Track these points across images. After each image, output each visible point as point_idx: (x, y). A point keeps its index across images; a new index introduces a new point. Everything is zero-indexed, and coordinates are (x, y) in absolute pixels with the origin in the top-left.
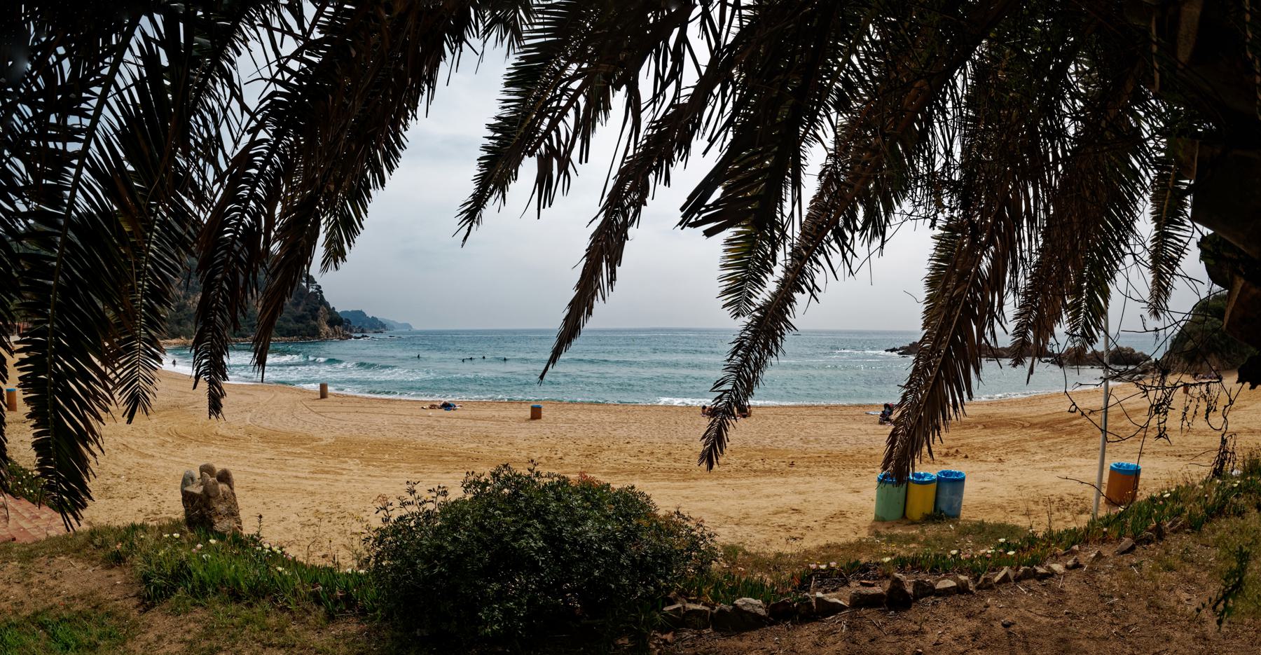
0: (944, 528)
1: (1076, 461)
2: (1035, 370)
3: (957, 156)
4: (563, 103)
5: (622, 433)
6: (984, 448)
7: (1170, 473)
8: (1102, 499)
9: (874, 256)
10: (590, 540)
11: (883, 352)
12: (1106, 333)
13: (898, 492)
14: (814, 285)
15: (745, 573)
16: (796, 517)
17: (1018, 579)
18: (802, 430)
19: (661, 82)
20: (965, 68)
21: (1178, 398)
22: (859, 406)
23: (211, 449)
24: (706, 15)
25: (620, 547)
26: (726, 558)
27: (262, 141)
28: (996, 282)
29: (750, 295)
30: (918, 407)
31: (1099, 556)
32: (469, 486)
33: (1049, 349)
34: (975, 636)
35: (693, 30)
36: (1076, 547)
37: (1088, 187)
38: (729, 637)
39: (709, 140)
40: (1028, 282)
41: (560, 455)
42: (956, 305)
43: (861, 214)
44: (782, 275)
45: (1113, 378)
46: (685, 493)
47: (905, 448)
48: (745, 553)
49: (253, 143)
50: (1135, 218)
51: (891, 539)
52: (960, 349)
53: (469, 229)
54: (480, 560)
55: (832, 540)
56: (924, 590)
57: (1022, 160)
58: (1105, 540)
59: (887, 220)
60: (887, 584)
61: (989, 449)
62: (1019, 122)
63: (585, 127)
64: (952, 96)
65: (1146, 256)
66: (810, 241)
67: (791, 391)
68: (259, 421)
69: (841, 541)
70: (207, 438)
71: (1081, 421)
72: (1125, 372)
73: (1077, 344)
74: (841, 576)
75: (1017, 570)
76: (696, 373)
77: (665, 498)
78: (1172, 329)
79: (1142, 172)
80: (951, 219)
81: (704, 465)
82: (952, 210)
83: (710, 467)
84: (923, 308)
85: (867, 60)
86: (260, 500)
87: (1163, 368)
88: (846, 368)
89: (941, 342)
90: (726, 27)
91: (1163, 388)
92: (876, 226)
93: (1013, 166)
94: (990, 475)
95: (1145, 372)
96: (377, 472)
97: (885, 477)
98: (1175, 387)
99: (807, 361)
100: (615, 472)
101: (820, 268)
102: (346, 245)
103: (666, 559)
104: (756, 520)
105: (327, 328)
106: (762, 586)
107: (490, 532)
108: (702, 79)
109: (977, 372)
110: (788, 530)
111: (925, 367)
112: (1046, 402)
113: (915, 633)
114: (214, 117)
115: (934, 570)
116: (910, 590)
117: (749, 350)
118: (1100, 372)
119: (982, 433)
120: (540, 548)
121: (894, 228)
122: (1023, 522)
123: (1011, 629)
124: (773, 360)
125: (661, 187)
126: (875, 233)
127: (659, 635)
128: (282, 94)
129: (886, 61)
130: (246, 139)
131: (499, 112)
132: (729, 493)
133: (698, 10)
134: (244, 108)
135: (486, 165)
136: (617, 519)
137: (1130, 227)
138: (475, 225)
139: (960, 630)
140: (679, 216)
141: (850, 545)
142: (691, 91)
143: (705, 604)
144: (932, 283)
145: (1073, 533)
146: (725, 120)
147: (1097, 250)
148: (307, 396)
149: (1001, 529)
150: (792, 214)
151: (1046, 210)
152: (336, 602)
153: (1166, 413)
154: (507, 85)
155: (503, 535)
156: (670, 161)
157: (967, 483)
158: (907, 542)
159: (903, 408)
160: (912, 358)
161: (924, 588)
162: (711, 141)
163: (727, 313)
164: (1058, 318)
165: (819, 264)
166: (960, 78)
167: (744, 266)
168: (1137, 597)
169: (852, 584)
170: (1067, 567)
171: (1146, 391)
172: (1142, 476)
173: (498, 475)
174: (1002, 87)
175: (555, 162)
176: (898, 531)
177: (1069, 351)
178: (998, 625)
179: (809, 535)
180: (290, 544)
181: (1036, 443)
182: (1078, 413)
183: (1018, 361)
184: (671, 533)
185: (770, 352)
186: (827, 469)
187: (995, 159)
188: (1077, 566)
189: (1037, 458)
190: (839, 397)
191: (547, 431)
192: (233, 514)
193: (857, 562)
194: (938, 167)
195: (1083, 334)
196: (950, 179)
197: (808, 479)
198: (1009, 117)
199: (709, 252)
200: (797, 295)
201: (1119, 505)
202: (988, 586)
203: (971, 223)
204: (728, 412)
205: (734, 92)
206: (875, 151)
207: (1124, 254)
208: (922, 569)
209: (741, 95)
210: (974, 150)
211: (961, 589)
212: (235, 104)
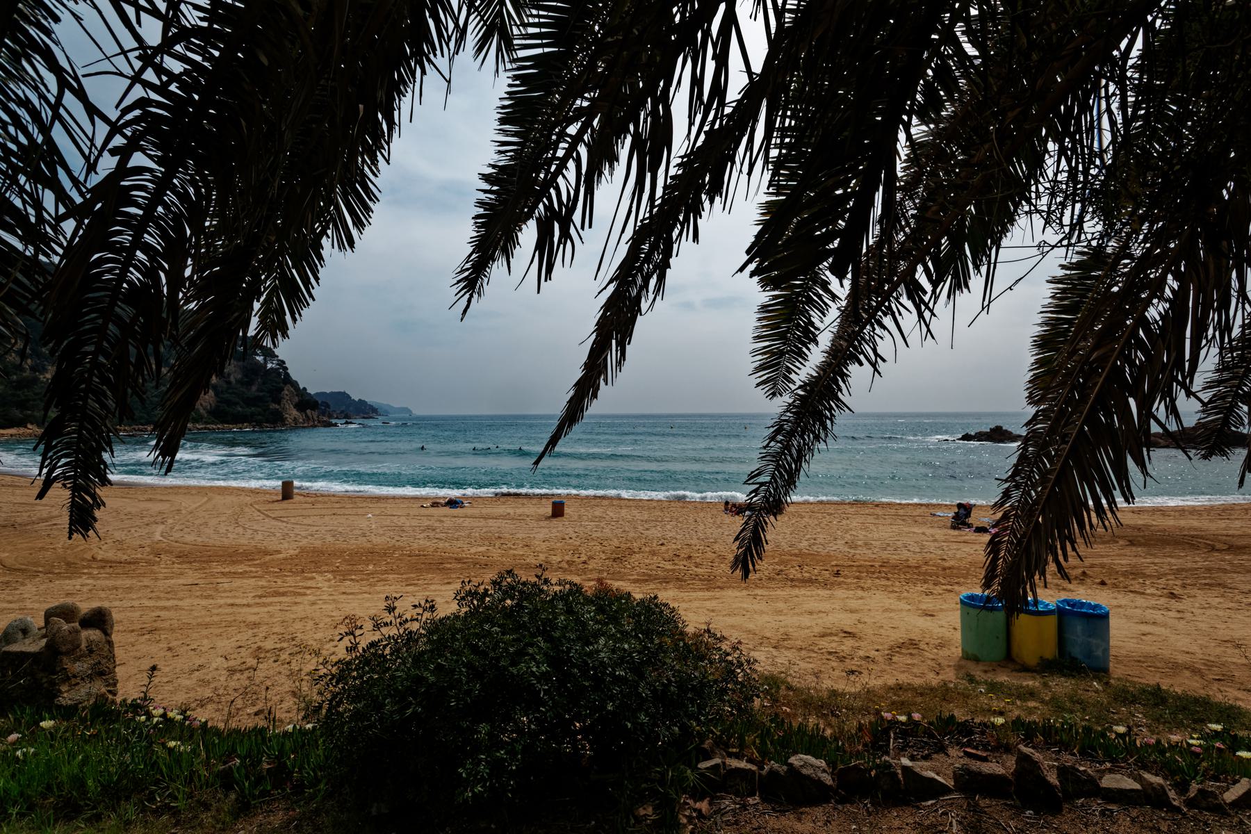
4: (560, 153)
5: (655, 533)
6: (1135, 573)
10: (602, 663)
16: (849, 643)
18: (847, 532)
23: (79, 581)
25: (638, 670)
27: (140, 170)
29: (789, 370)
32: (463, 598)
38: (783, 812)
41: (584, 558)
46: (708, 604)
48: (789, 688)
49: (122, 170)
53: (469, 301)
54: (468, 693)
55: (904, 678)
56: (1082, 787)
60: (1011, 762)
61: (1145, 576)
63: (590, 180)
68: (177, 535)
69: (917, 682)
70: (71, 568)
74: (932, 736)
77: (695, 611)
81: (738, 573)
86: (164, 645)
96: (356, 588)
100: (646, 579)
102: (288, 317)
104: (799, 643)
105: (295, 412)
107: (484, 654)
110: (842, 659)
111: (1038, 455)
114: (35, 115)
116: (1053, 778)
117: (791, 434)
119: (1127, 551)
120: (543, 674)
127: (690, 802)
128: (159, 105)
130: (108, 164)
131: (493, 158)
132: (762, 606)
134: (93, 111)
135: (483, 225)
136: (636, 637)
138: (475, 296)
141: (932, 689)
143: (750, 761)
144: (1043, 343)
148: (261, 498)
152: (260, 780)
154: (503, 121)
155: (498, 659)
157: (1114, 622)
163: (761, 393)
165: (884, 328)
167: (782, 336)
169: (954, 752)
173: (499, 584)
175: (556, 226)
180: (202, 704)
184: (702, 658)
185: (817, 438)
186: (884, 582)
191: (570, 530)
192: (101, 674)
197: (860, 593)
200: (853, 368)
208: (1066, 746)
211: (1152, 798)
212: (69, 99)
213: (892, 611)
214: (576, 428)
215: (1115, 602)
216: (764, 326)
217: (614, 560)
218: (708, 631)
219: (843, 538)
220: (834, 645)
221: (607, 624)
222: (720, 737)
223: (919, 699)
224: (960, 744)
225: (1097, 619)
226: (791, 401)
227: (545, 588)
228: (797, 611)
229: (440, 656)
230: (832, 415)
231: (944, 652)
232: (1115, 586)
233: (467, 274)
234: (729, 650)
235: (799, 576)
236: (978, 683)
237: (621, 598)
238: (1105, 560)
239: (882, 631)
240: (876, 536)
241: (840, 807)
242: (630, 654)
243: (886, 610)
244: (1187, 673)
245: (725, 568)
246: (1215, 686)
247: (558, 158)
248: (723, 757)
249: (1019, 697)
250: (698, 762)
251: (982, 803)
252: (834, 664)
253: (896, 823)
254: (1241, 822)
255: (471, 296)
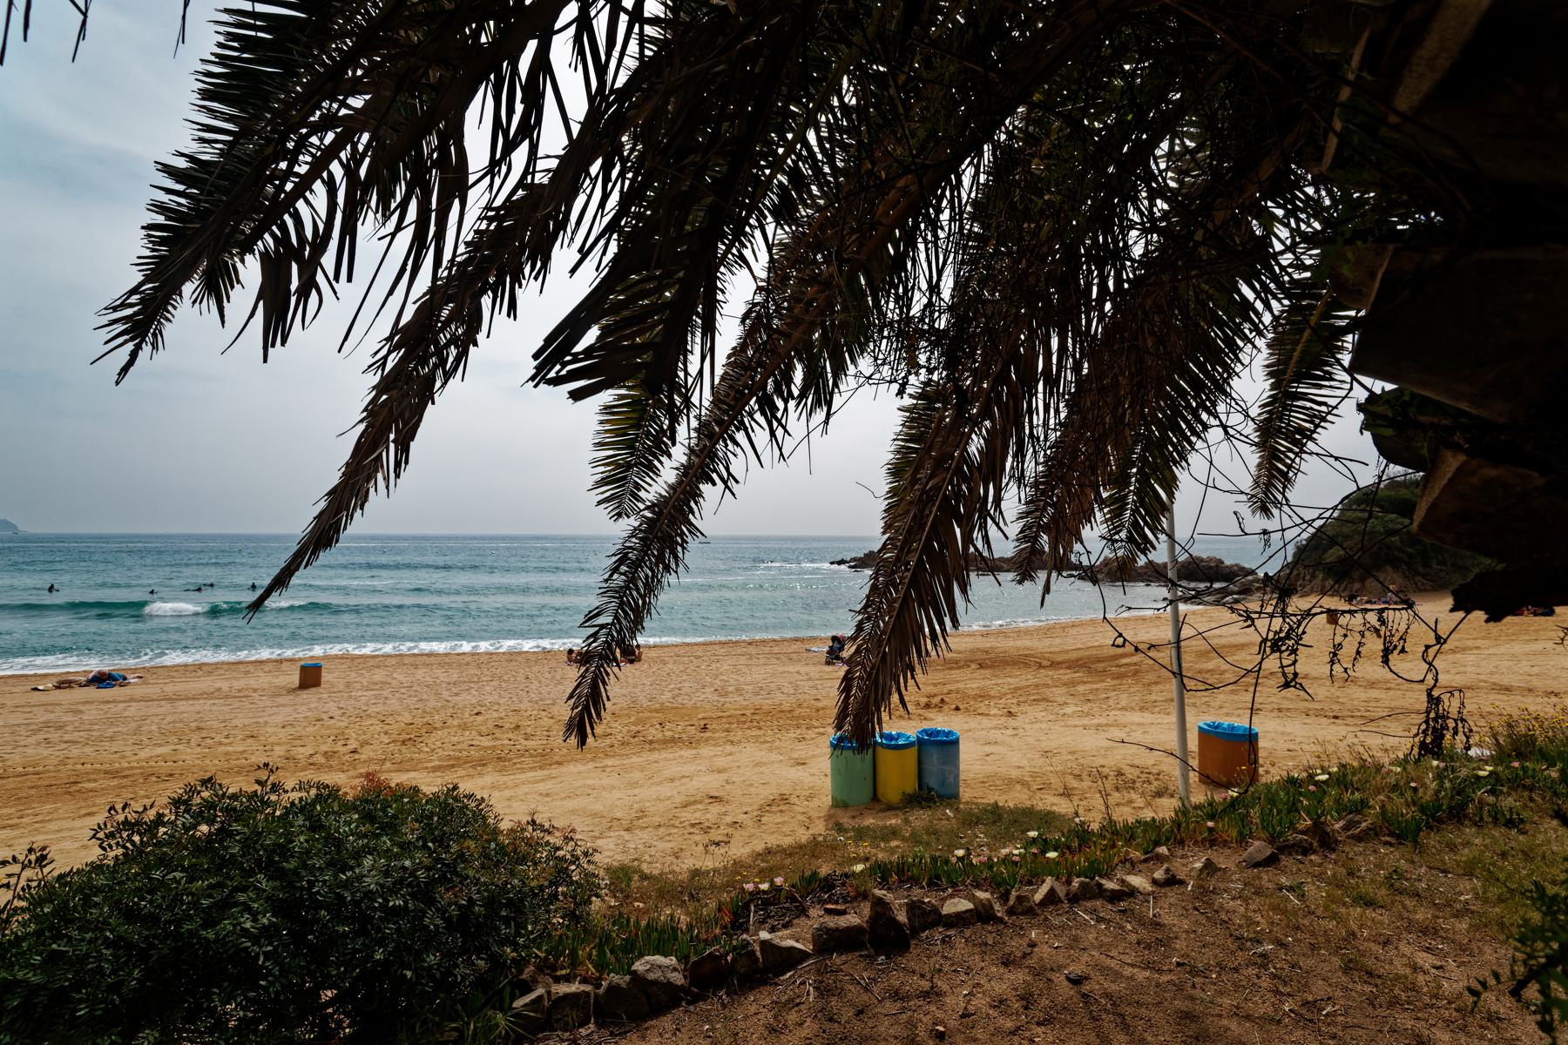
0: (938, 814)
1: (1136, 717)
2: (1053, 587)
3: (946, 294)
4: (302, 169)
5: (468, 698)
6: (983, 696)
7: (1317, 742)
8: (1194, 777)
9: (815, 435)
10: (369, 895)
11: (827, 565)
12: (1171, 537)
13: (861, 762)
14: (729, 474)
15: (646, 911)
16: (716, 809)
17: (1074, 899)
18: (717, 676)
19: (505, 141)
20: (980, 155)
21: (1317, 632)
22: (796, 640)
24: (584, 23)
26: (614, 889)
28: (991, 469)
29: (638, 487)
30: (880, 641)
31: (1209, 866)
32: (111, 835)
33: (1073, 559)
34: (1027, 1000)
35: (562, 49)
36: (1163, 850)
37: (1152, 333)
39: (580, 251)
40: (1040, 468)
41: (353, 745)
42: (931, 500)
43: (798, 376)
44: (684, 460)
45: (1186, 600)
46: (542, 787)
47: (866, 698)
48: (644, 877)
50: (1231, 373)
51: (861, 834)
52: (937, 560)
53: (133, 356)
54: (115, 988)
55: (773, 841)
56: (925, 918)
57: (1047, 298)
58: (1213, 841)
59: (836, 385)
60: (866, 909)
61: (990, 697)
62: (1051, 240)
64: (951, 202)
65: (1249, 429)
66: (725, 412)
67: (698, 621)
69: (786, 841)
71: (1136, 659)
72: (1208, 591)
73: (1120, 553)
74: (794, 900)
75: (1069, 882)
76: (557, 601)
77: (510, 800)
78: (1297, 530)
79: (1259, 305)
80: (928, 383)
81: (573, 740)
82: (930, 371)
83: (583, 741)
84: (884, 505)
85: (831, 139)
87: (1282, 587)
88: (775, 589)
89: (909, 552)
90: (616, 54)
91: (1284, 615)
92: (820, 394)
93: (1031, 306)
94: (996, 735)
95: (1246, 591)
97: (840, 739)
98: (1308, 614)
99: (720, 579)
101: (738, 450)
103: (511, 907)
104: (657, 819)
106: (675, 930)
107: (151, 920)
108: (573, 145)
109: (964, 591)
111: (886, 585)
112: (1073, 631)
113: (925, 995)
115: (934, 884)
116: (902, 917)
117: (636, 565)
118: (1163, 592)
121: (846, 396)
122: (1063, 807)
123: (1086, 988)
124: (671, 579)
125: (501, 318)
126: (817, 403)
129: (860, 142)
132: (613, 780)
133: (570, 12)
136: (425, 846)
137: (1221, 388)
138: (147, 349)
139: (1000, 988)
140: (530, 366)
141: (801, 847)
142: (554, 163)
143: (584, 981)
144: (896, 471)
145: (1152, 825)
146: (606, 220)
147: (1158, 423)
149: (1026, 816)
150: (701, 372)
151: (1077, 368)
153: (1294, 652)
154: (206, 94)
156: (517, 279)
157: (963, 746)
158: (885, 839)
159: (859, 641)
160: (869, 572)
161: (925, 914)
162: (584, 253)
163: (603, 512)
164: (1088, 516)
165: (737, 444)
166: (970, 171)
167: (630, 445)
168: (1313, 947)
169: (815, 912)
170: (1155, 882)
171: (1248, 618)
172: (1262, 743)
174: (1035, 186)
176: (869, 821)
177: (1107, 562)
178: (1059, 979)
179: (738, 836)
181: (1064, 690)
182: (1129, 649)
183: (1025, 575)
184: (523, 860)
185: (667, 568)
186: (756, 732)
187: (1003, 298)
188: (1172, 881)
189: (1069, 710)
190: (766, 628)
193: (815, 874)
194: (916, 310)
195: (1130, 539)
196: (931, 326)
197: (729, 748)
198: (1035, 234)
199: (576, 424)
200: (705, 488)
201: (1227, 786)
202: (1024, 909)
203: (958, 389)
204: (606, 657)
205: (622, 175)
206: (825, 284)
207: (1206, 427)
208: (915, 881)
209: (633, 180)
210: (974, 284)
211: (982, 915)
213: (764, 764)
214: (325, 557)
215: (966, 727)
216: (607, 431)
217: (403, 743)
218: (534, 822)
219: (712, 685)
220: (698, 815)
221: (378, 836)
222: (546, 958)
223: (788, 861)
224: (822, 902)
225: (947, 745)
226: (636, 524)
227: (273, 798)
228: (656, 779)
229: (57, 937)
230: (684, 541)
231: (816, 803)
232: (967, 710)
233: (129, 311)
234: (559, 843)
235: (660, 736)
236: (846, 831)
237: (403, 796)
238: (960, 685)
239: (752, 790)
240: (749, 679)
241: (692, 1008)
242: (413, 874)
243: (757, 764)
244: (1018, 787)
245: (558, 732)
246: (1039, 795)
247: (297, 175)
248: (548, 985)
249: (883, 840)
250: (513, 999)
251: (838, 961)
252: (697, 838)
253: (753, 1009)
254: (1046, 919)
255: (138, 348)
